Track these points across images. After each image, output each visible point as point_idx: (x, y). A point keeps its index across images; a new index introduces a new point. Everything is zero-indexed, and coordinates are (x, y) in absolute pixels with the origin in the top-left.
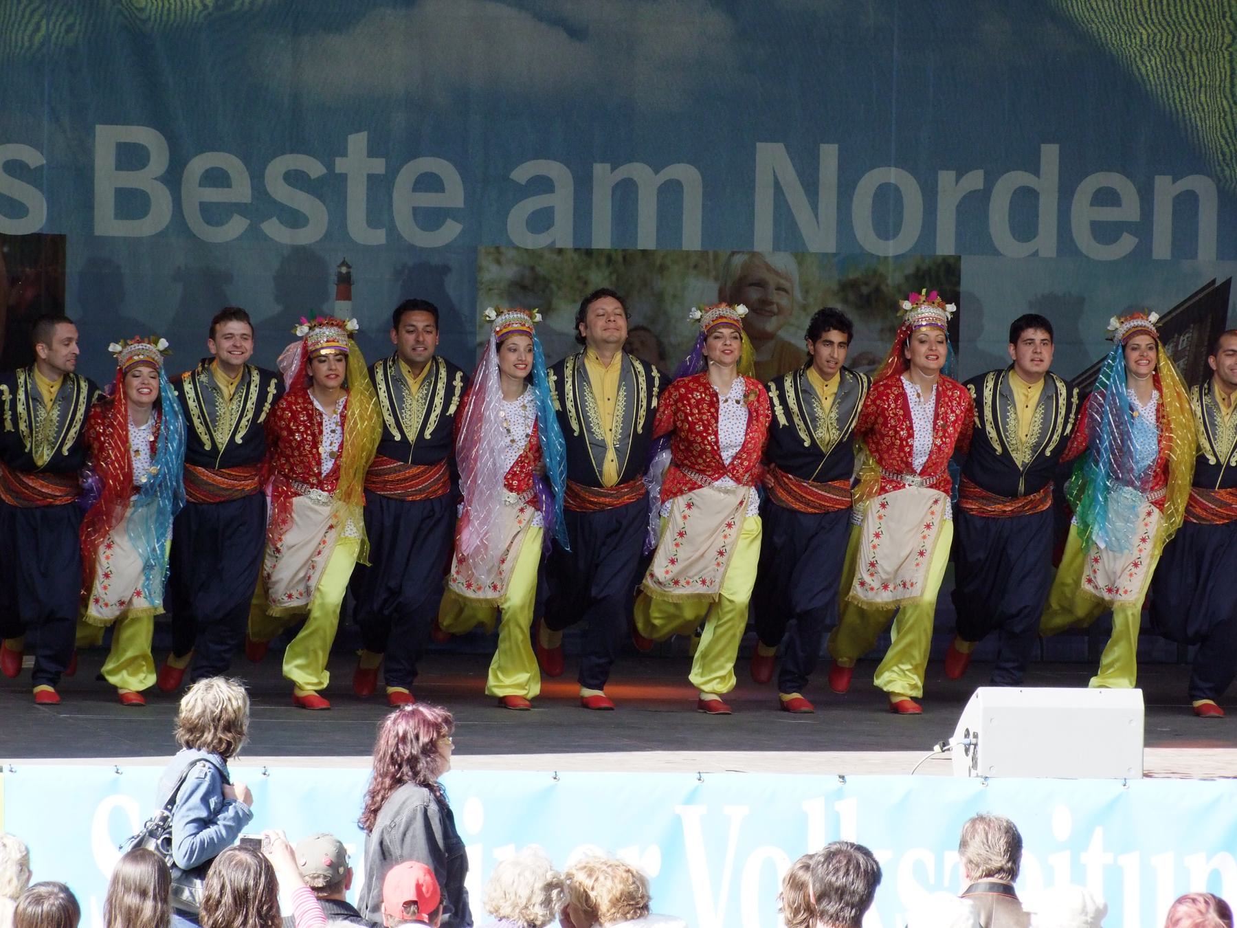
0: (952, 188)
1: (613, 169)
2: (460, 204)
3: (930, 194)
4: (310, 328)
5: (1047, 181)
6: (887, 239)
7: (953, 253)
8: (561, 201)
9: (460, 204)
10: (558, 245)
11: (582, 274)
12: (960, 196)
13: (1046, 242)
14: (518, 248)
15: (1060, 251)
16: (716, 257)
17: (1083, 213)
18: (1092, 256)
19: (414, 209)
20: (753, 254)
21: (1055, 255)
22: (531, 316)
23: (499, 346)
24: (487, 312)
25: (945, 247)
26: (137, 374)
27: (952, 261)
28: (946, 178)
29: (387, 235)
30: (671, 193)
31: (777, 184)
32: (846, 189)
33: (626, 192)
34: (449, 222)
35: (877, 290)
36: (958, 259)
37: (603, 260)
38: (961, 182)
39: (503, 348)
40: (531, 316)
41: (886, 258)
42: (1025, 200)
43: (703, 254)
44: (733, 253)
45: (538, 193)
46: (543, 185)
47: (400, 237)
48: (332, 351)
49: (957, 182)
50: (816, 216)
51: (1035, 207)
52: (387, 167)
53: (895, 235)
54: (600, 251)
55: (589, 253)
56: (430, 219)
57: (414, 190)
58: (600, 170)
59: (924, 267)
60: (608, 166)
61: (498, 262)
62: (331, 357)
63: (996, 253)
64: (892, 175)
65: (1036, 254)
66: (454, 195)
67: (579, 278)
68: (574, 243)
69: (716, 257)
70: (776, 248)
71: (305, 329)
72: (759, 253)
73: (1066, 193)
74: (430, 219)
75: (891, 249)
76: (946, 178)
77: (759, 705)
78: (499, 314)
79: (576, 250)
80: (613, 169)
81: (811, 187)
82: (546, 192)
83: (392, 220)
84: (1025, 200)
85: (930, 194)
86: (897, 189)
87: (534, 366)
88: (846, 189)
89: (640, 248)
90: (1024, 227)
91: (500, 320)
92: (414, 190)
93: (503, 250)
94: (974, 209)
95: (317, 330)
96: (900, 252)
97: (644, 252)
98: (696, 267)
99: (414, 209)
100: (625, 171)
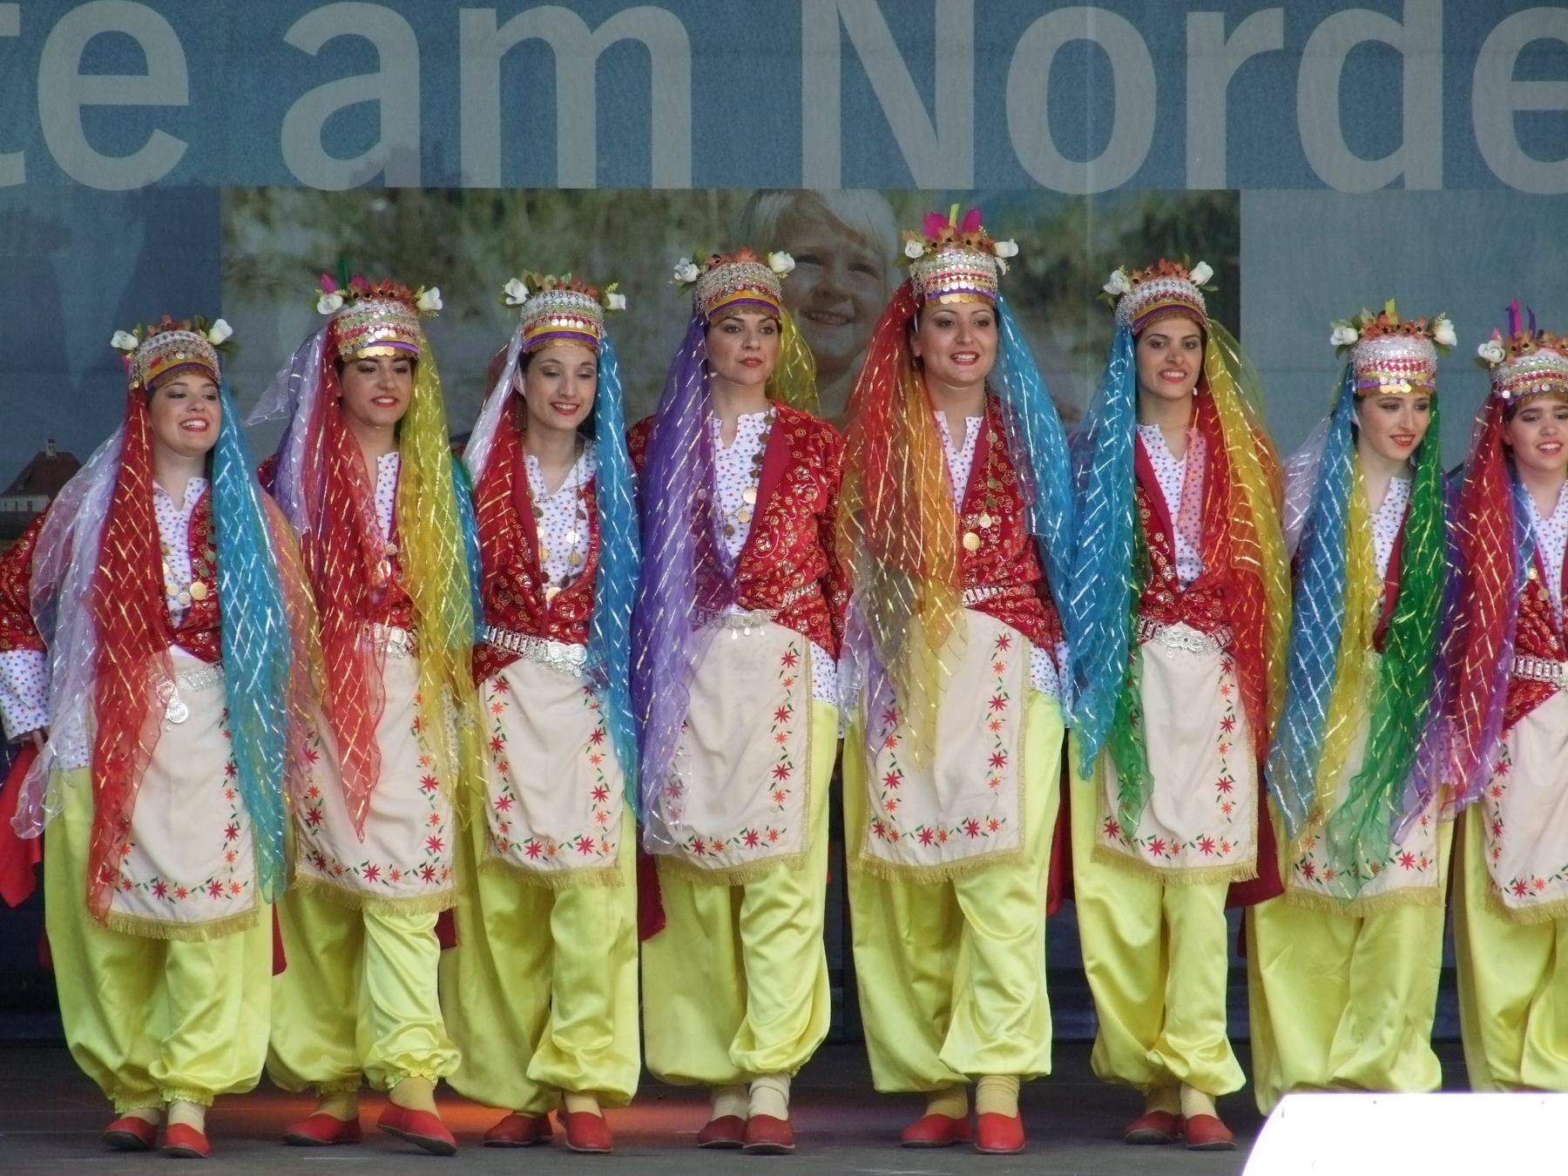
0: (1215, 51)
1: (501, 21)
2: (183, 99)
3: (1171, 61)
4: (346, 300)
5: (1419, 33)
6: (1080, 157)
7: (1221, 185)
8: (395, 87)
9: (183, 99)
10: (390, 183)
11: (442, 240)
12: (1234, 64)
13: (1420, 157)
14: (303, 189)
15: (1449, 179)
16: (724, 204)
17: (1498, 95)
18: (1518, 185)
19: (84, 109)
20: (801, 195)
21: (1437, 185)
22: (601, 299)
23: (525, 360)
24: (508, 289)
25: (1206, 172)
26: (178, 389)
27: (1218, 202)
28: (1203, 26)
29: (28, 165)
30: (624, 68)
31: (848, 52)
32: (993, 55)
33: (529, 68)
34: (159, 137)
35: (1064, 264)
36: (1234, 196)
37: (486, 212)
38: (1236, 34)
39: (534, 366)
40: (601, 299)
41: (1080, 199)
42: (1374, 67)
43: (697, 197)
44: (760, 193)
45: (341, 74)
46: (354, 55)
47: (53, 168)
48: (389, 351)
49: (1227, 35)
50: (931, 112)
51: (1396, 87)
52: (24, 21)
53: (1100, 149)
54: (479, 194)
55: (455, 196)
56: (114, 130)
57: (83, 70)
58: (475, 22)
59: (1161, 216)
60: (490, 14)
61: (264, 219)
62: (386, 364)
63: (1311, 181)
64: (1092, 24)
65: (1399, 182)
66: (167, 78)
67: (435, 251)
68: (424, 177)
69: (724, 204)
70: (850, 180)
71: (336, 300)
72: (814, 193)
73: (1460, 55)
74: (114, 130)
75: (1088, 179)
76: (1203, 26)
77: (825, 1139)
78: (534, 290)
79: (428, 191)
80: (501, 21)
81: (918, 50)
82: (360, 71)
83: (39, 134)
84: (1374, 67)
85: (1171, 61)
86: (1099, 52)
87: (597, 405)
88: (993, 55)
89: (563, 183)
90: (1374, 127)
91: (534, 306)
92: (83, 70)
93: (274, 193)
94: (1265, 88)
95: (360, 305)
96: (1114, 183)
97: (568, 192)
98: (681, 224)
99: (84, 109)
100: (524, 26)
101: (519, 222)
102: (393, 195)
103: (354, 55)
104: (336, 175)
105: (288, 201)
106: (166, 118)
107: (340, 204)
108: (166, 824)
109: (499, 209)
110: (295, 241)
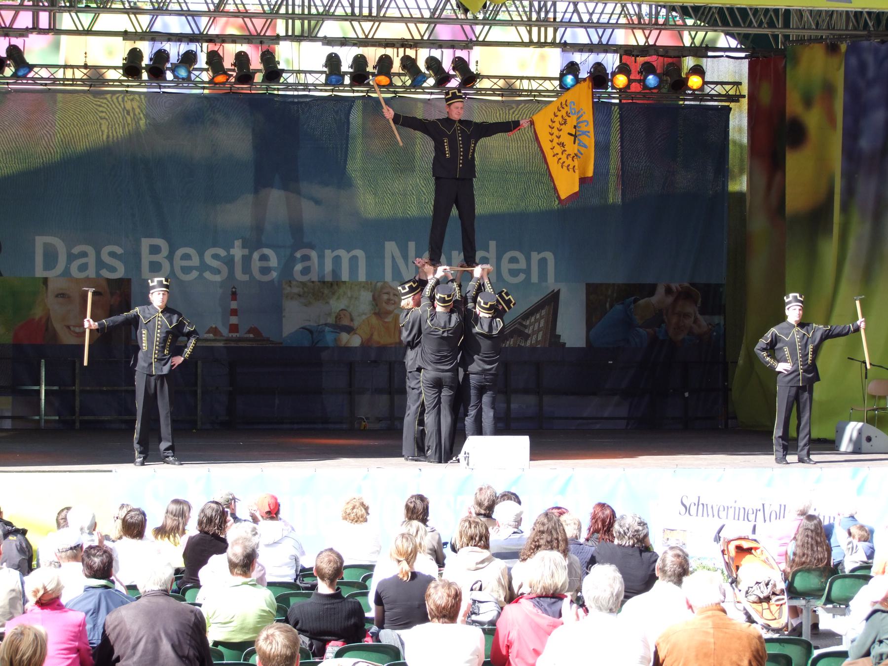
20: (385, 282)
30: (354, 260)
43: (367, 283)
46: (84, 254)
47: (254, 278)
70: (393, 280)
100: (336, 253)
101: (335, 287)
102: (313, 282)
103: (84, 254)
104: (305, 279)
105: (294, 283)
106: (195, 268)
107: (303, 284)
108: (580, 529)
109: (332, 285)
110: (296, 290)
